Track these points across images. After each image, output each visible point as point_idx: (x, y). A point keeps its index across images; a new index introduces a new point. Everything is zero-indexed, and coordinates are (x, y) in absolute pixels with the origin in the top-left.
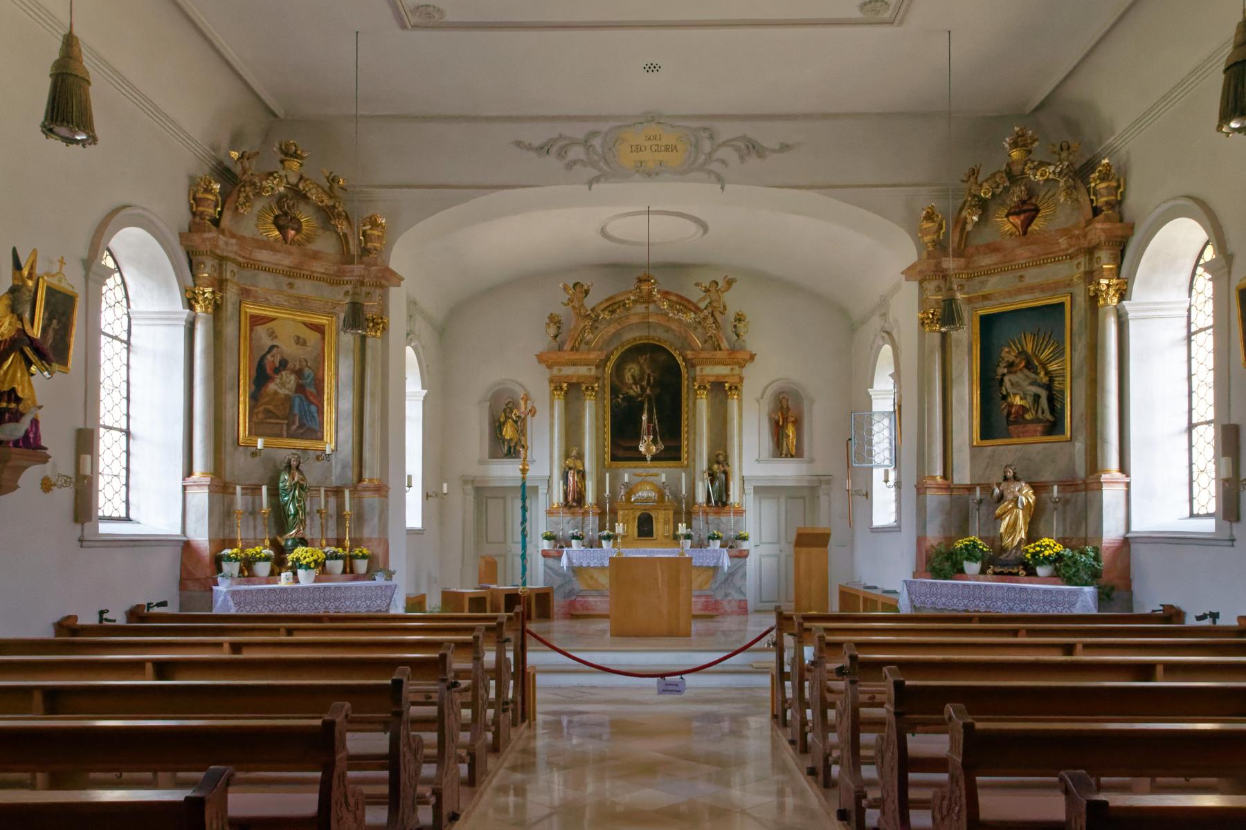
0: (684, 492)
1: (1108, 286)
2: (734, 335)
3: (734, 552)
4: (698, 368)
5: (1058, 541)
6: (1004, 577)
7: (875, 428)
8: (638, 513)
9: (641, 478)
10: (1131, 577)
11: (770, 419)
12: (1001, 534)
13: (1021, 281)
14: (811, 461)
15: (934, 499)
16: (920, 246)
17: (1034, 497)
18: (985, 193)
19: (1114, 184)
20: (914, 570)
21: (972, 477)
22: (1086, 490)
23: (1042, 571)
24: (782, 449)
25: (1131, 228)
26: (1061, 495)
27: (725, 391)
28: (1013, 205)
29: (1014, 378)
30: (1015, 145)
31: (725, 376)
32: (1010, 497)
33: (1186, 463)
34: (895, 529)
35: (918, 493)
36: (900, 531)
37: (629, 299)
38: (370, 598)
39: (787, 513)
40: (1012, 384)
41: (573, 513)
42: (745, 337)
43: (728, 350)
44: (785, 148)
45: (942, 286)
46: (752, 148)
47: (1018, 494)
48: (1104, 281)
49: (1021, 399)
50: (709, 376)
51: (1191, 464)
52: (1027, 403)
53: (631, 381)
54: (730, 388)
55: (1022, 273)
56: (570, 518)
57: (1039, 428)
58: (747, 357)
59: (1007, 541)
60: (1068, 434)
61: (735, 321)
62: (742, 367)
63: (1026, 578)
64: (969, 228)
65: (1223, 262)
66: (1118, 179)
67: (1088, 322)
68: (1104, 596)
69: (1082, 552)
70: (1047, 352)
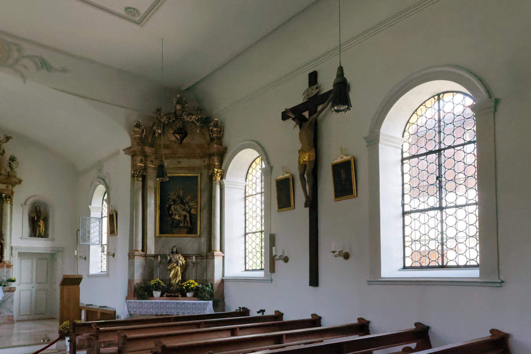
1: (217, 172)
2: (9, 168)
3: (6, 288)
5: (196, 281)
7: (92, 225)
10: (224, 296)
11: (29, 217)
12: (170, 278)
14: (53, 240)
15: (139, 261)
16: (133, 139)
17: (185, 261)
19: (219, 129)
20: (127, 296)
21: (155, 251)
22: (207, 258)
23: (189, 295)
24: (36, 233)
25: (226, 149)
27: (3, 198)
28: (176, 129)
29: (175, 207)
30: (178, 103)
32: (174, 261)
33: (244, 249)
34: (106, 275)
35: (129, 258)
36: (108, 276)
39: (37, 268)
40: (174, 209)
42: (16, 170)
43: (5, 175)
44: (64, 70)
45: (143, 160)
46: (44, 65)
47: (178, 259)
48: (216, 170)
49: (179, 217)
51: (245, 249)
52: (182, 218)
54: (6, 197)
55: (180, 160)
57: (185, 230)
58: (17, 181)
59: (173, 281)
60: (199, 234)
61: (10, 160)
62: (13, 186)
63: (182, 298)
64: (157, 135)
65: (269, 169)
66: (221, 128)
68: (215, 306)
69: (207, 286)
70: (189, 197)
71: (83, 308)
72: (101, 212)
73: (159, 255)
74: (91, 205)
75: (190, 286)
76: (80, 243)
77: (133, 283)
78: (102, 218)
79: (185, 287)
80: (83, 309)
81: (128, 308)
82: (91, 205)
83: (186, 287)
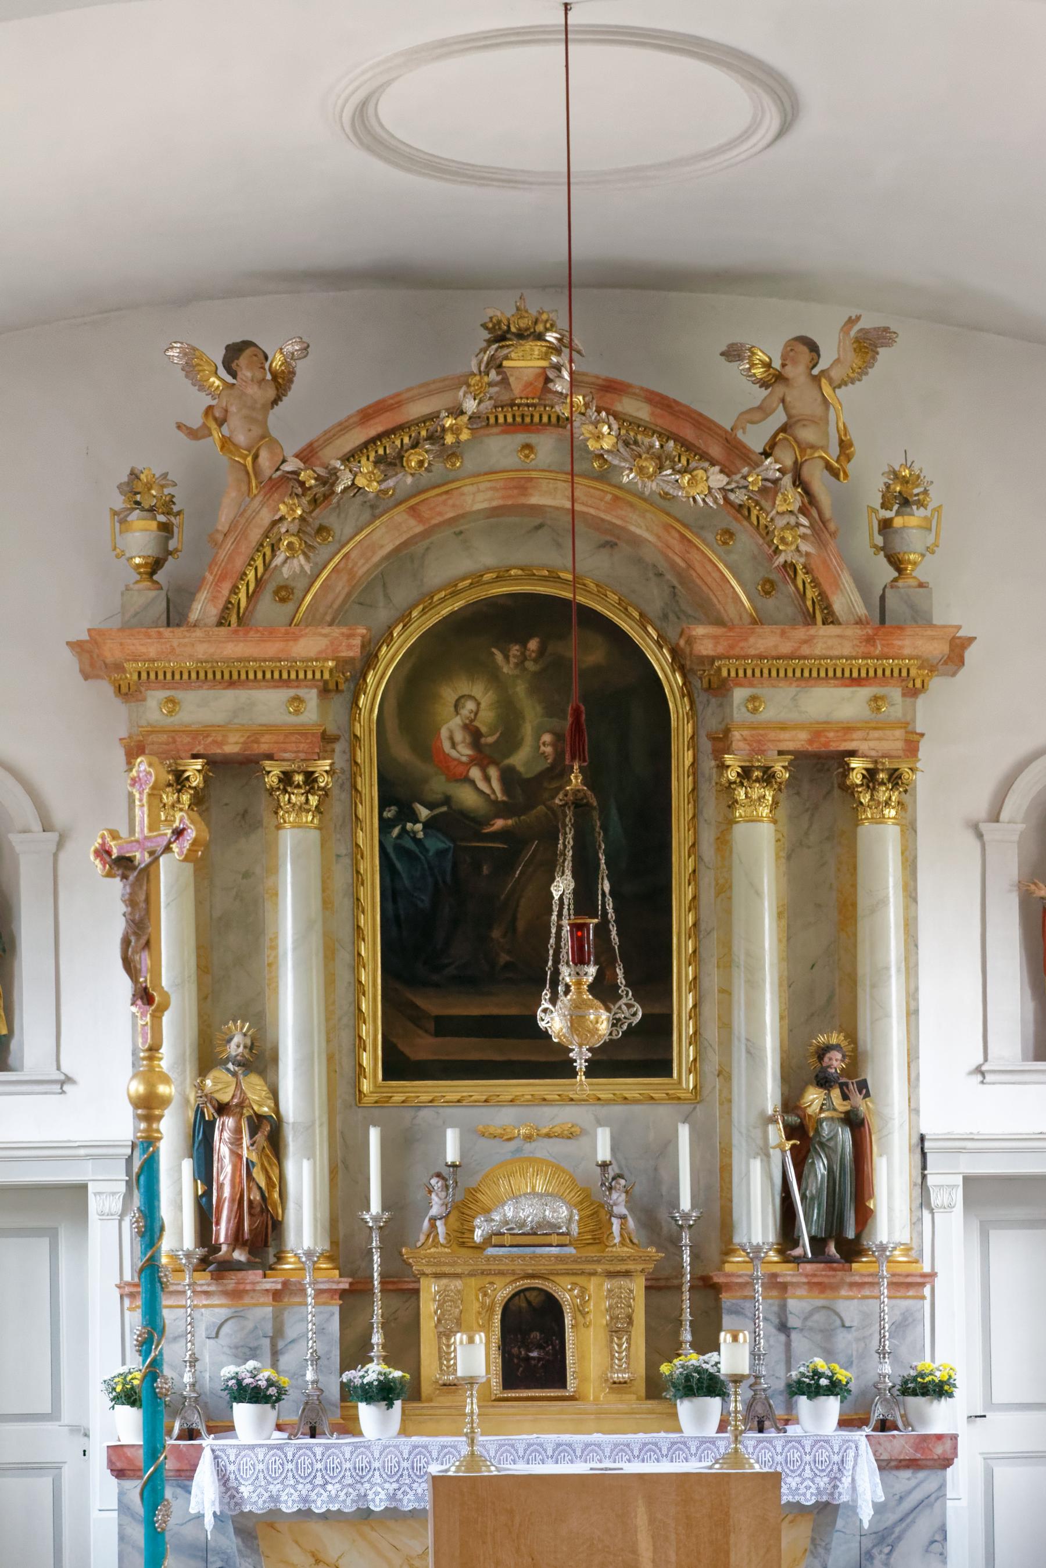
0: (685, 1203)
4: (739, 694)
8: (502, 1291)
9: (512, 1145)
31: (847, 729)
37: (458, 411)
41: (236, 1295)
50: (783, 727)
53: (465, 752)
54: (871, 775)
56: (223, 1313)
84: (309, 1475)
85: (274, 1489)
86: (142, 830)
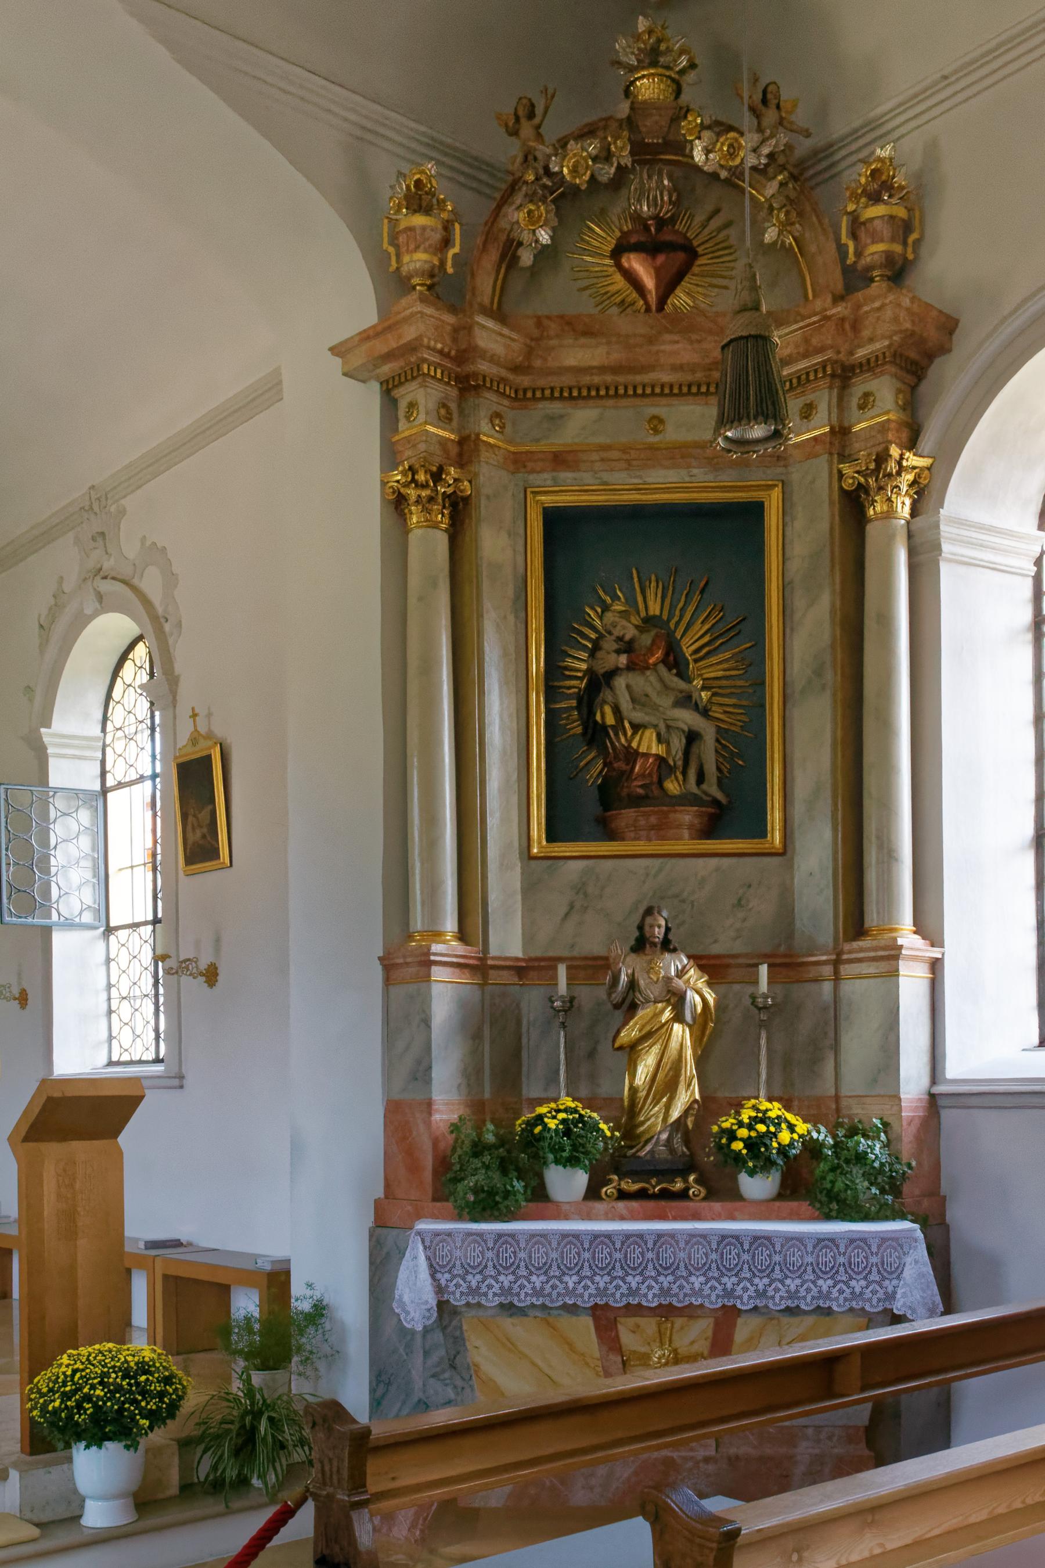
6: (650, 1205)
7: (58, 831)
13: (656, 431)
18: (574, 171)
20: (380, 1193)
21: (528, 939)
26: (778, 989)
29: (639, 681)
38: (671, 1269)
40: (633, 700)
55: (659, 410)
60: (776, 838)
64: (526, 258)
67: (837, 549)
71: (140, 1261)
72: (99, 763)
73: (560, 959)
74: (49, 726)
75: (775, 1135)
76: (7, 918)
77: (428, 1123)
78: (104, 791)
79: (742, 1139)
80: (140, 1266)
81: (433, 1272)
82: (49, 727)
83: (749, 1143)
84: (576, 1264)
85: (729, 1282)
86: (539, 842)
